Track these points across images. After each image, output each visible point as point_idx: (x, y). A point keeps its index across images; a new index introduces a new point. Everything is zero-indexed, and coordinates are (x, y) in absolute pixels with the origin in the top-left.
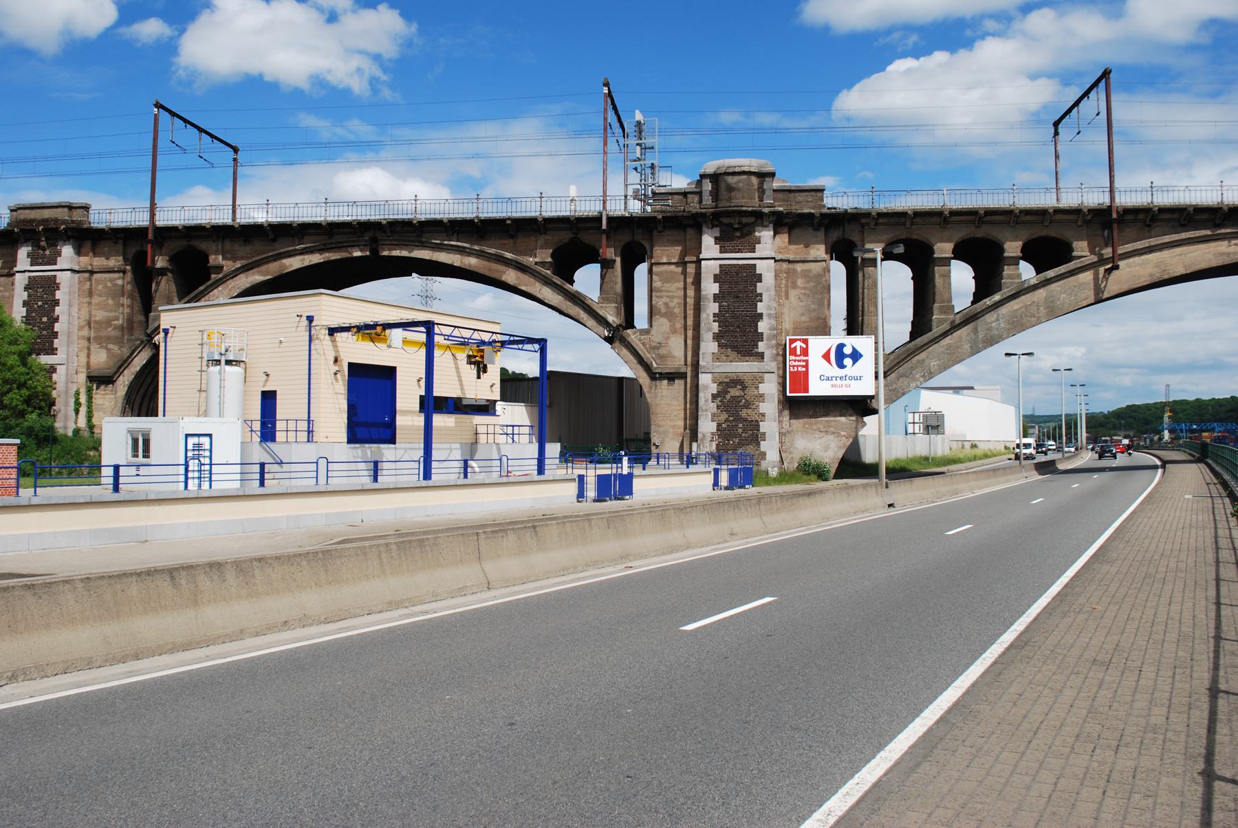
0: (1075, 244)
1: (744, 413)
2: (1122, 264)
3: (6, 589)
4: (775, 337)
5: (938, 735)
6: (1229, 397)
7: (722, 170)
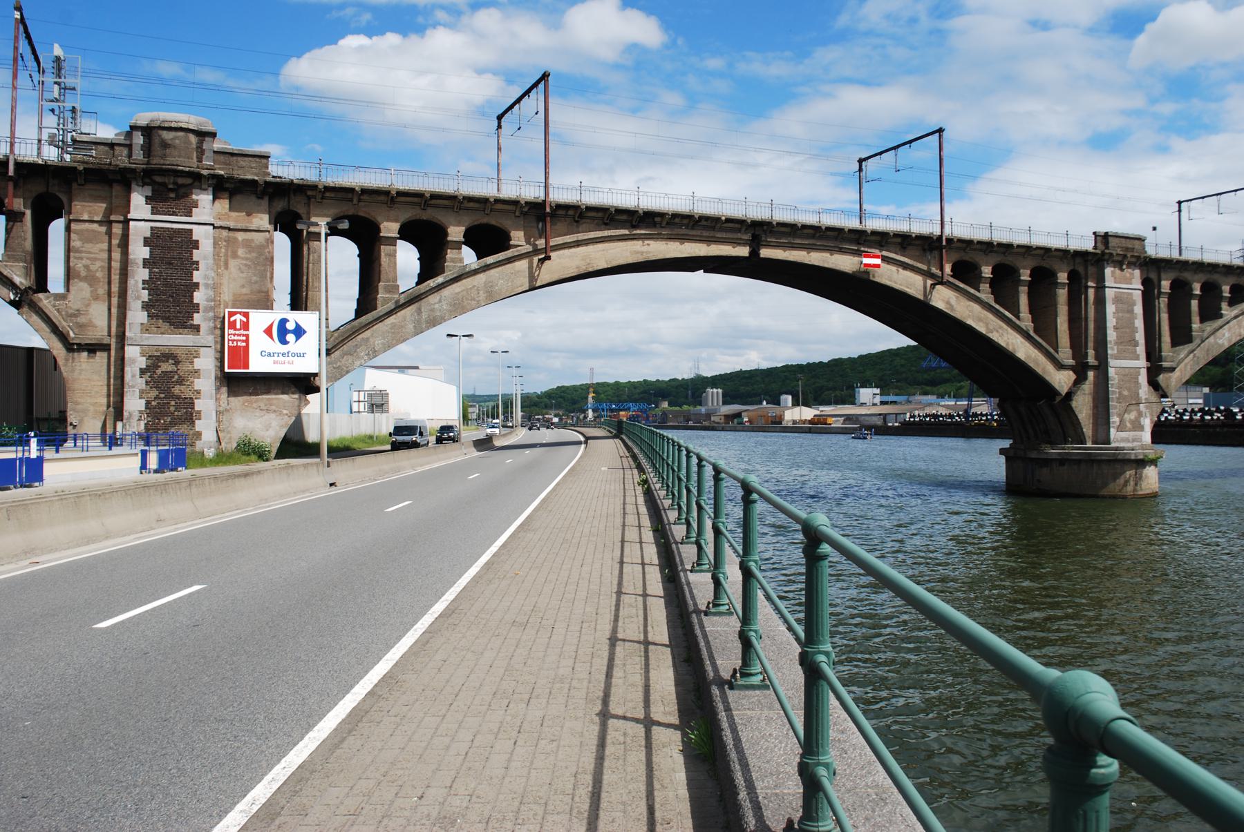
0: (513, 234)
1: (176, 390)
2: (553, 255)
4: (212, 309)
5: (364, 708)
6: (642, 380)
7: (157, 124)
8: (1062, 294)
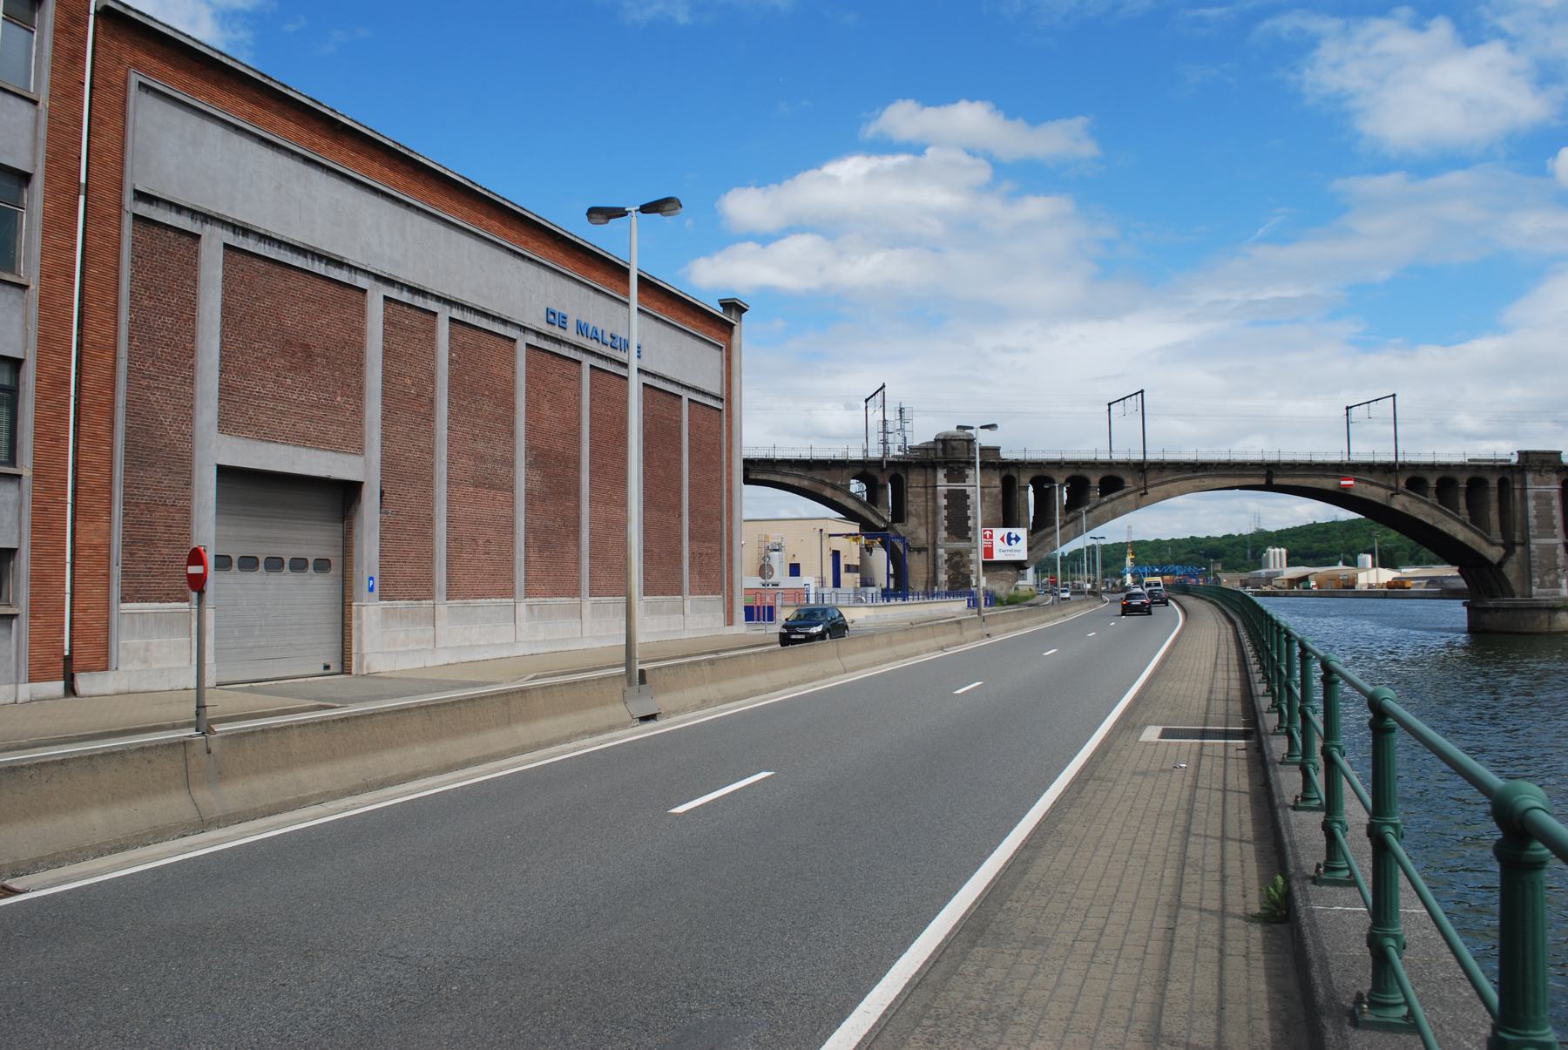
1: (962, 570)
3: (13, 769)
7: (949, 438)
8: (1493, 495)
